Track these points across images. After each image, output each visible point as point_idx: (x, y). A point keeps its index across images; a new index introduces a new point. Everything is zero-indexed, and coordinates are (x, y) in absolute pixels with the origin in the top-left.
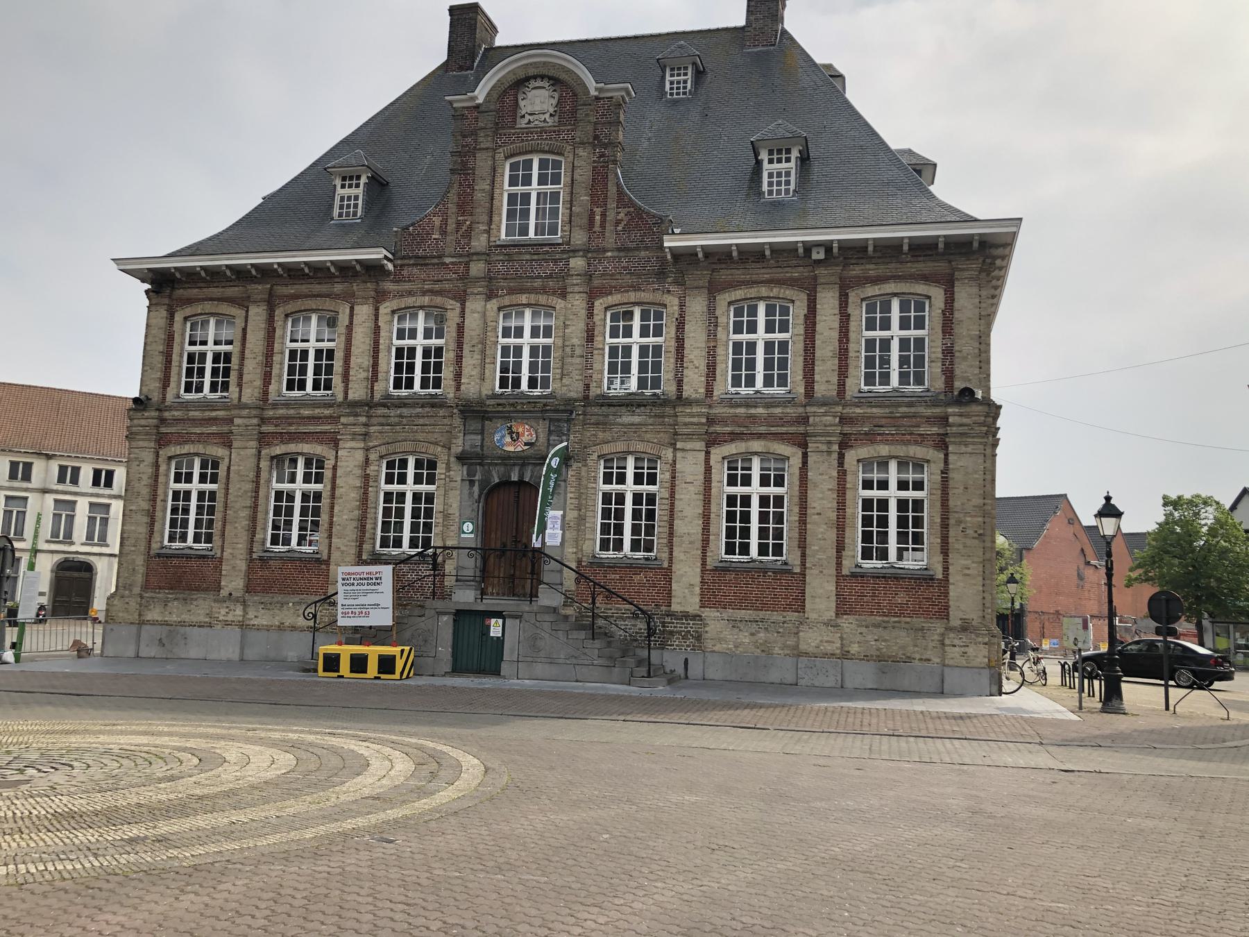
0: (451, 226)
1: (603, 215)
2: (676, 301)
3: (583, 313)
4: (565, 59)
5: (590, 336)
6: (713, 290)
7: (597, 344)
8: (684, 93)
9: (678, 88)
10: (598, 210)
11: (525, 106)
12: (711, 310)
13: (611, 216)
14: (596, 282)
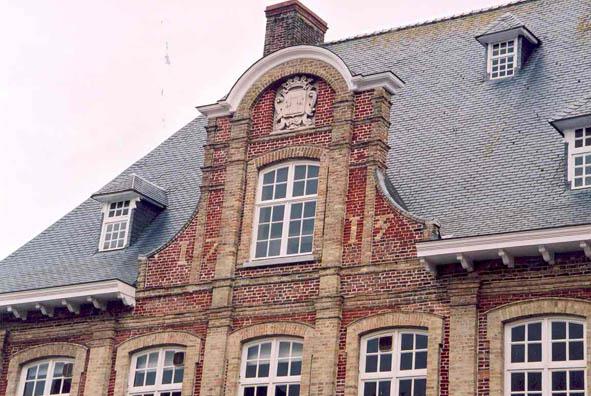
0: (198, 250)
1: (360, 224)
2: (439, 322)
3: (333, 342)
4: (327, 56)
5: (341, 370)
6: (483, 305)
7: (349, 381)
8: (510, 72)
9: (503, 68)
10: (354, 220)
11: (281, 110)
12: (481, 331)
13: (368, 224)
14: (349, 304)
